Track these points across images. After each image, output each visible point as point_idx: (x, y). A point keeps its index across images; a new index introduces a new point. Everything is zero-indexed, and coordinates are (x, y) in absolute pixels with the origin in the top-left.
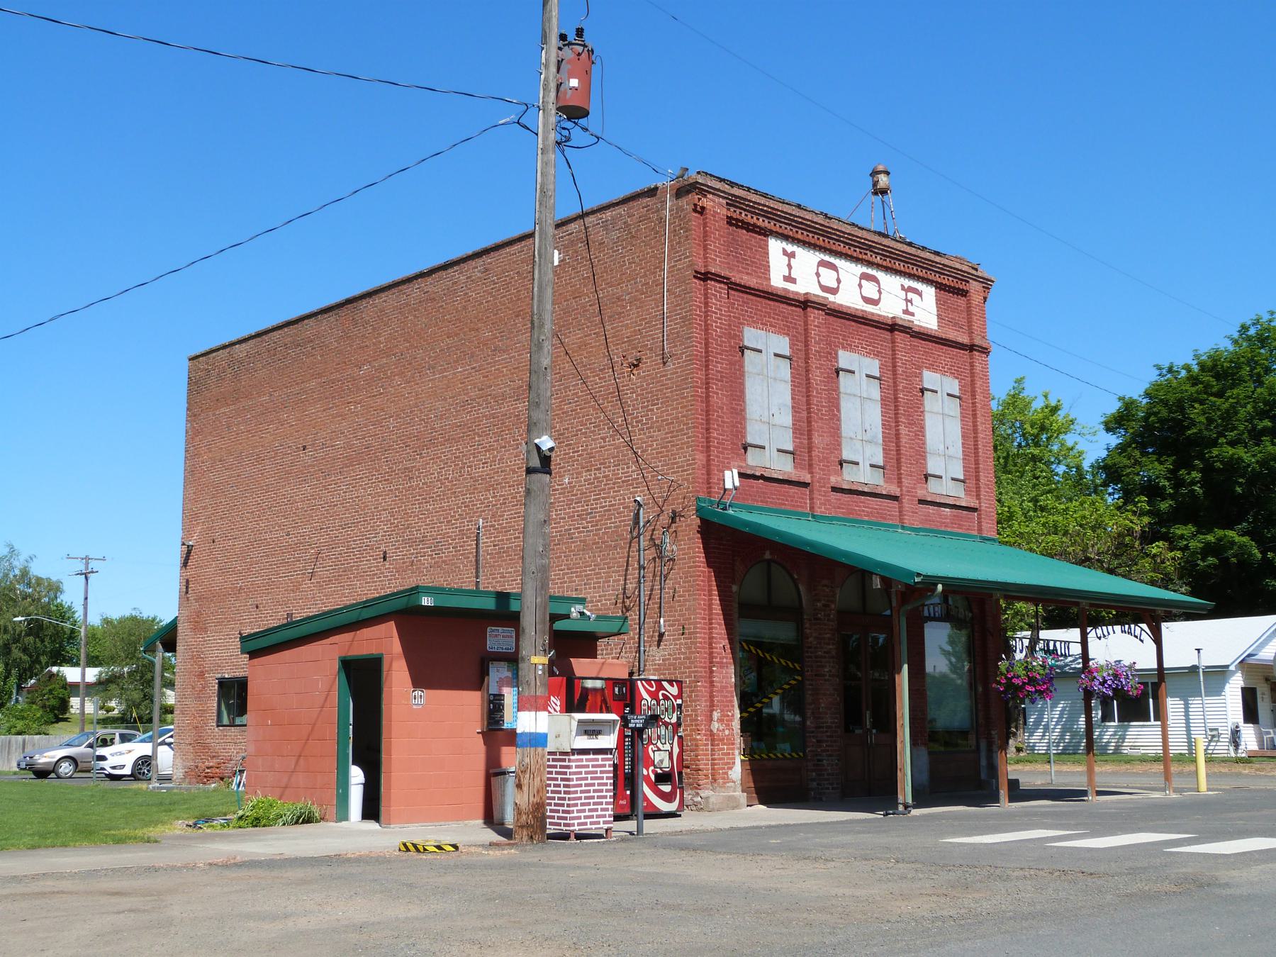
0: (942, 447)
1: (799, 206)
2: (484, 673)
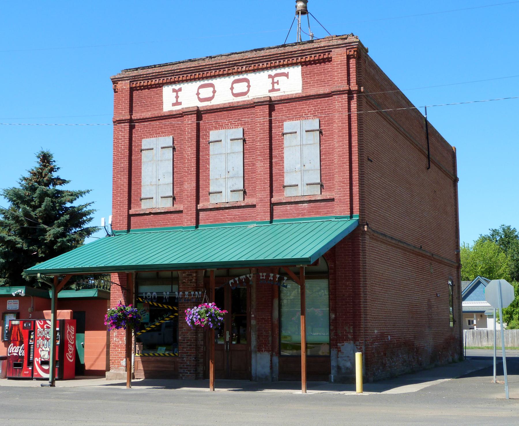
0: (299, 166)
1: (190, 60)
2: (3, 319)
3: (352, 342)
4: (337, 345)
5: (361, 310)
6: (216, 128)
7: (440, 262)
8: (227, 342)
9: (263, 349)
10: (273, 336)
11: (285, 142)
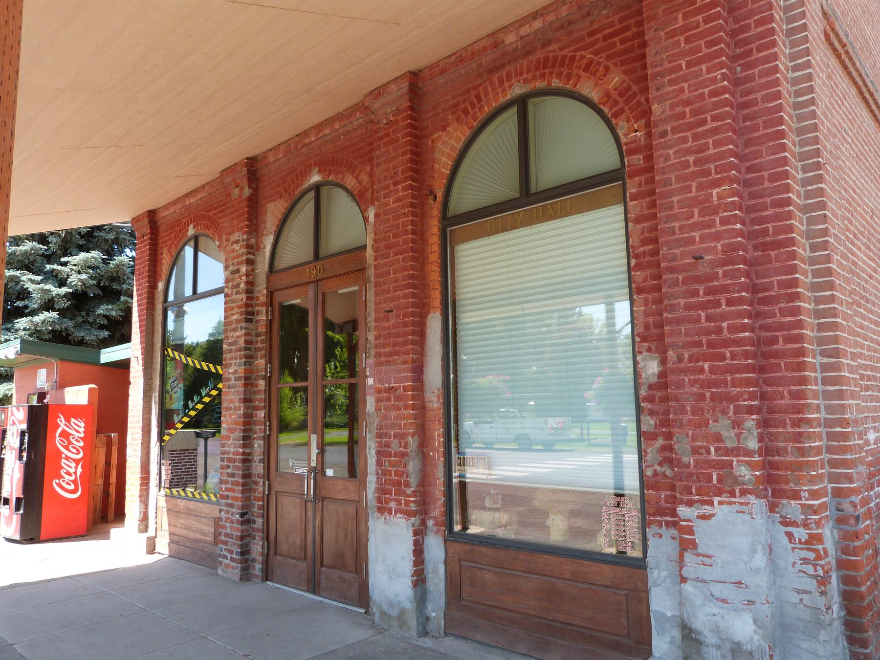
3: (758, 504)
4: (674, 513)
5: (800, 325)
9: (393, 505)
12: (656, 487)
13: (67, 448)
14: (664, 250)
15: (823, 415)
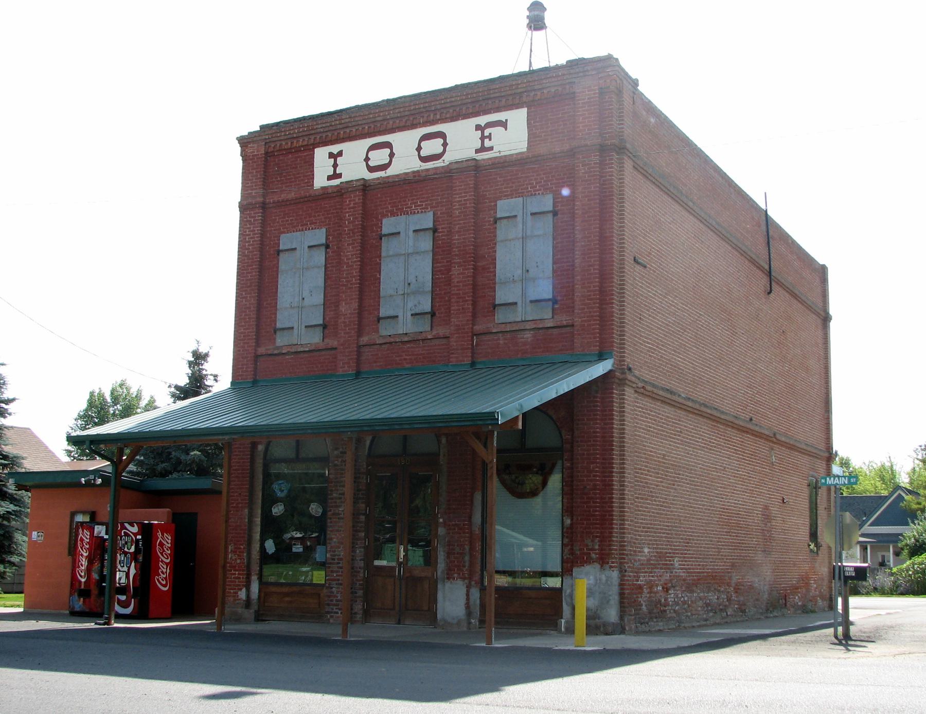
6: (393, 214)
7: (792, 447)
8: (400, 564)
9: (456, 575)
10: (471, 556)
11: (498, 232)
12: (567, 562)
13: (162, 554)
14: (575, 482)
15: (619, 539)
